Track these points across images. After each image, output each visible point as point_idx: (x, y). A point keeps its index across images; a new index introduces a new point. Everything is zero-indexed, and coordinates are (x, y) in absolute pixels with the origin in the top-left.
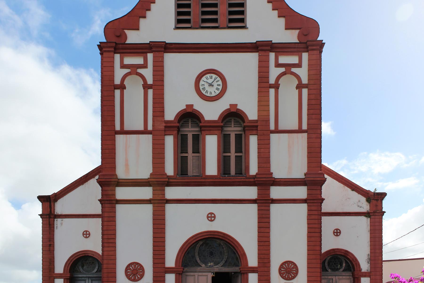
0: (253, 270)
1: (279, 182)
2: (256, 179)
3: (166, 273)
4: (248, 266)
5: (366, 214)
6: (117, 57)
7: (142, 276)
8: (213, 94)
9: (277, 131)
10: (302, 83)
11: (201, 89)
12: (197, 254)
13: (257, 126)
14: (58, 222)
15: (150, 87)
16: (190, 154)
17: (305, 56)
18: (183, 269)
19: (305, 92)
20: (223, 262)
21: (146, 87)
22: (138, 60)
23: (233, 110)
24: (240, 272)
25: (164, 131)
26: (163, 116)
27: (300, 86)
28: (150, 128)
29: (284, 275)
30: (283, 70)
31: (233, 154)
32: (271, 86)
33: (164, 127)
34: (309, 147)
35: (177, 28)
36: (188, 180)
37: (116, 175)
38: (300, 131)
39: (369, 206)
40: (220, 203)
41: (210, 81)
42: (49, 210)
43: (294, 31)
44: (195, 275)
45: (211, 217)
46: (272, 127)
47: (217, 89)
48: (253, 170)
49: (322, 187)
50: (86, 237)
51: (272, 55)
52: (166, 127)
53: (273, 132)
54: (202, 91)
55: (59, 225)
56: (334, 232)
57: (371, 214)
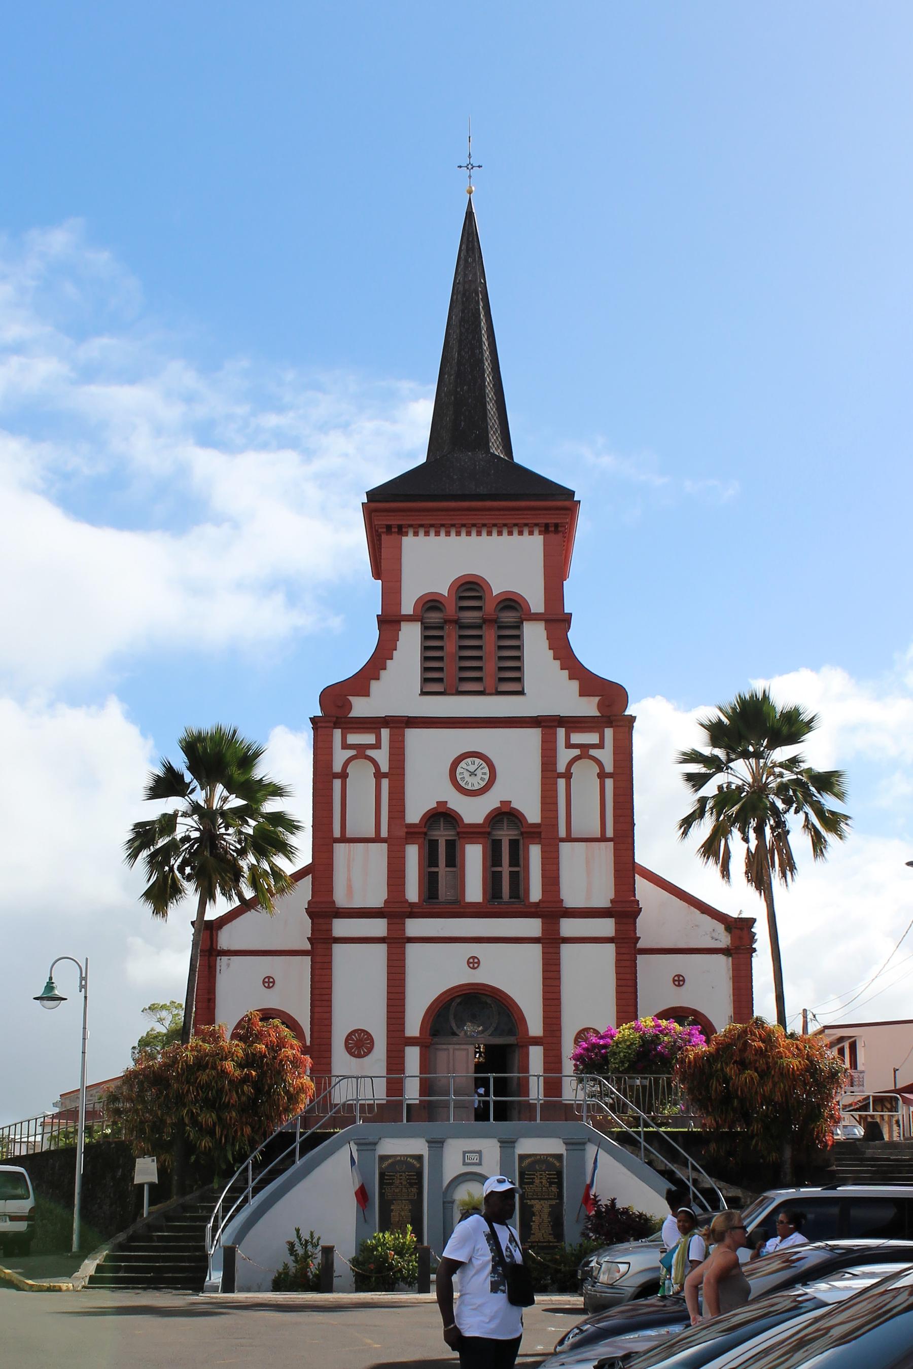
0: (536, 1041)
1: (573, 912)
2: (538, 909)
3: (406, 1046)
4: (528, 1035)
5: (725, 952)
6: (337, 733)
7: (370, 1050)
8: (477, 787)
9: (569, 839)
10: (604, 771)
11: (459, 780)
12: (451, 1017)
13: (540, 833)
14: (222, 962)
15: (385, 775)
16: (442, 868)
17: (609, 733)
18: (432, 1040)
19: (609, 783)
20: (492, 1029)
21: (379, 775)
22: (368, 739)
23: (505, 810)
24: (517, 1045)
25: (404, 840)
26: (403, 817)
27: (602, 775)
28: (384, 833)
29: (357, 1035)
30: (577, 752)
31: (506, 869)
32: (561, 775)
33: (404, 834)
34: (616, 863)
35: (423, 693)
36: (439, 910)
37: (334, 902)
38: (603, 839)
39: (730, 938)
40: (419, 719)
41: (472, 768)
42: (209, 943)
43: (592, 698)
44: (468, 1049)
45: (474, 963)
46: (562, 833)
47: (482, 779)
48: (535, 894)
49: (637, 920)
50: (269, 987)
51: (561, 732)
52: (407, 833)
53: (563, 840)
54: (460, 782)
55: (224, 968)
56: (674, 981)
57: (732, 952)
